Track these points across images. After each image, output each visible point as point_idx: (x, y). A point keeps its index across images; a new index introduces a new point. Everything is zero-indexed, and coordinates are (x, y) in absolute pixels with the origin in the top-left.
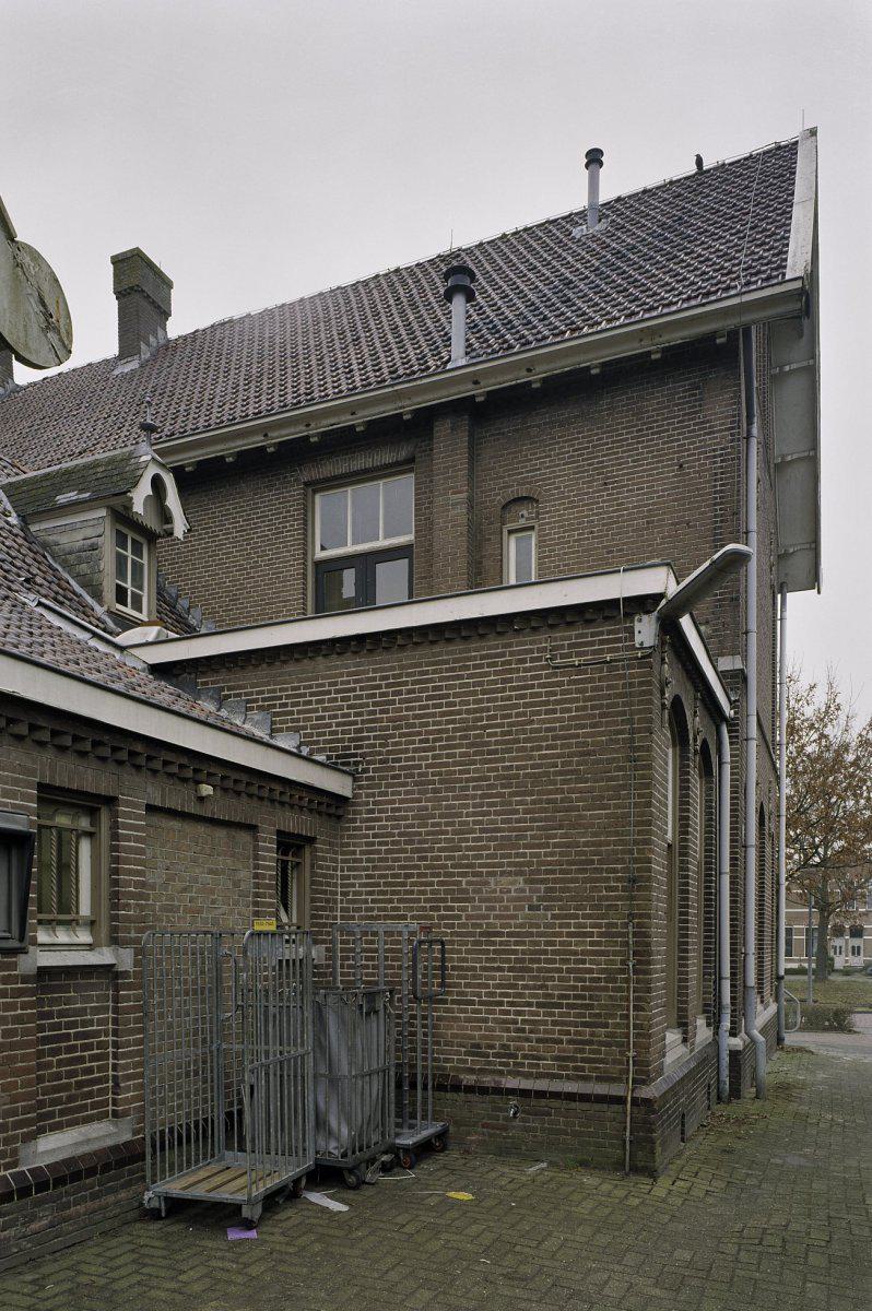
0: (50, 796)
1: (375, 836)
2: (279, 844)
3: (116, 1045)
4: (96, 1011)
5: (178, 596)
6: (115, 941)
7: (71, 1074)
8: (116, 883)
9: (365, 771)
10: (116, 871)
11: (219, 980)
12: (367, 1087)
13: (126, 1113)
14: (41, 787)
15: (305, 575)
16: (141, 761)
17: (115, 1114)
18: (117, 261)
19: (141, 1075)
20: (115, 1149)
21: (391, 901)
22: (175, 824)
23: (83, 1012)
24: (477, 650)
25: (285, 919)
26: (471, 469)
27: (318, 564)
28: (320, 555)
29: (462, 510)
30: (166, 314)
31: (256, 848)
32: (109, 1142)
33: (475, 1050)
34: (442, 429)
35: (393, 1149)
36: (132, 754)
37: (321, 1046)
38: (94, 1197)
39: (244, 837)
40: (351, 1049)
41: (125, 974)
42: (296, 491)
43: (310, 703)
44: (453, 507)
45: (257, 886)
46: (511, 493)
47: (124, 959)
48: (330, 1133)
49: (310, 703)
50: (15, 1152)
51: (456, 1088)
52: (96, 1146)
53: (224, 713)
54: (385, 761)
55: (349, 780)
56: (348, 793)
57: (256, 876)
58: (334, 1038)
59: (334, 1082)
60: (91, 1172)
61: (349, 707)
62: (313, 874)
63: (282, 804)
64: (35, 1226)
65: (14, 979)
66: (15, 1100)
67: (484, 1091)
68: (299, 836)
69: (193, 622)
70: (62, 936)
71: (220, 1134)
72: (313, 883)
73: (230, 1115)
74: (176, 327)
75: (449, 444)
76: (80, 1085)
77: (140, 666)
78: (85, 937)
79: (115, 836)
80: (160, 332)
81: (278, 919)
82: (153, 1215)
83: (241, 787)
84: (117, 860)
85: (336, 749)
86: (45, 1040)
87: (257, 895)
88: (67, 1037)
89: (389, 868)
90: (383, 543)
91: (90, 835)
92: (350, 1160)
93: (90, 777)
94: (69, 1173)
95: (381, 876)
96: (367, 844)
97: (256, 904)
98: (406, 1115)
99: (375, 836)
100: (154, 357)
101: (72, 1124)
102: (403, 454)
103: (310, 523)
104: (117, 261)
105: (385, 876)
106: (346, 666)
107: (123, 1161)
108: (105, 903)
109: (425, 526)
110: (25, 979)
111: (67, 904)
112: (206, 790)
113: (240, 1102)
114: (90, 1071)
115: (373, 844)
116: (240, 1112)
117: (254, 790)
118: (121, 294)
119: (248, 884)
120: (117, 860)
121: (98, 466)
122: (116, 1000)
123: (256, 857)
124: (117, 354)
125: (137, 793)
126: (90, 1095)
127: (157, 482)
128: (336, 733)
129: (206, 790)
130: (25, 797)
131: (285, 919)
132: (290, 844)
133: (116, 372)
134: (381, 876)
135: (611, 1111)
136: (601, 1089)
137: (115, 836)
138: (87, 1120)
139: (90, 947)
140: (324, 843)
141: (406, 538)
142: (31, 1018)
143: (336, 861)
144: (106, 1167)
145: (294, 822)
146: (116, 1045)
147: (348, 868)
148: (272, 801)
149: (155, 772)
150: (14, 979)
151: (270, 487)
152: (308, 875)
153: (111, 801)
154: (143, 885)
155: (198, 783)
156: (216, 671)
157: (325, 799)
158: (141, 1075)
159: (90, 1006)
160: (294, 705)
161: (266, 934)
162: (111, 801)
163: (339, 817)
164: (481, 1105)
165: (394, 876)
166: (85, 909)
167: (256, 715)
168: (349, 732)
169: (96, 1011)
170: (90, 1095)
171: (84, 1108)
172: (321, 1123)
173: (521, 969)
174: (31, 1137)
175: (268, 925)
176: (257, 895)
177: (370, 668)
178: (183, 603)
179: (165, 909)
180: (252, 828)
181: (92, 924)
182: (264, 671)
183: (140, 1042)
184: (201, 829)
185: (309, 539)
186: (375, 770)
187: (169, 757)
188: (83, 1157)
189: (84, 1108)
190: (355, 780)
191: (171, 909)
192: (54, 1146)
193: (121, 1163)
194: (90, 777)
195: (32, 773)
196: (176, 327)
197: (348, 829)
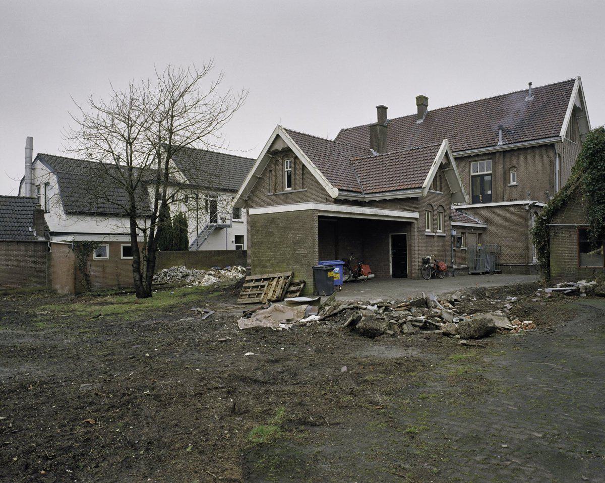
18: (417, 98)
24: (504, 209)
26: (503, 162)
27: (472, 176)
28: (473, 174)
29: (502, 169)
33: (505, 260)
34: (497, 155)
44: (500, 169)
46: (511, 166)
51: (503, 265)
67: (507, 266)
74: (429, 109)
75: (499, 158)
82: (470, 275)
90: (485, 173)
94: (464, 269)
98: (496, 269)
102: (489, 157)
104: (417, 98)
106: (486, 210)
107: (466, 269)
109: (494, 171)
132: (480, 234)
135: (524, 267)
136: (523, 264)
141: (491, 172)
145: (480, 232)
147: (487, 237)
159: (464, 252)
164: (506, 268)
173: (511, 250)
177: (489, 210)
192: (463, 266)
194: (464, 231)
196: (429, 109)
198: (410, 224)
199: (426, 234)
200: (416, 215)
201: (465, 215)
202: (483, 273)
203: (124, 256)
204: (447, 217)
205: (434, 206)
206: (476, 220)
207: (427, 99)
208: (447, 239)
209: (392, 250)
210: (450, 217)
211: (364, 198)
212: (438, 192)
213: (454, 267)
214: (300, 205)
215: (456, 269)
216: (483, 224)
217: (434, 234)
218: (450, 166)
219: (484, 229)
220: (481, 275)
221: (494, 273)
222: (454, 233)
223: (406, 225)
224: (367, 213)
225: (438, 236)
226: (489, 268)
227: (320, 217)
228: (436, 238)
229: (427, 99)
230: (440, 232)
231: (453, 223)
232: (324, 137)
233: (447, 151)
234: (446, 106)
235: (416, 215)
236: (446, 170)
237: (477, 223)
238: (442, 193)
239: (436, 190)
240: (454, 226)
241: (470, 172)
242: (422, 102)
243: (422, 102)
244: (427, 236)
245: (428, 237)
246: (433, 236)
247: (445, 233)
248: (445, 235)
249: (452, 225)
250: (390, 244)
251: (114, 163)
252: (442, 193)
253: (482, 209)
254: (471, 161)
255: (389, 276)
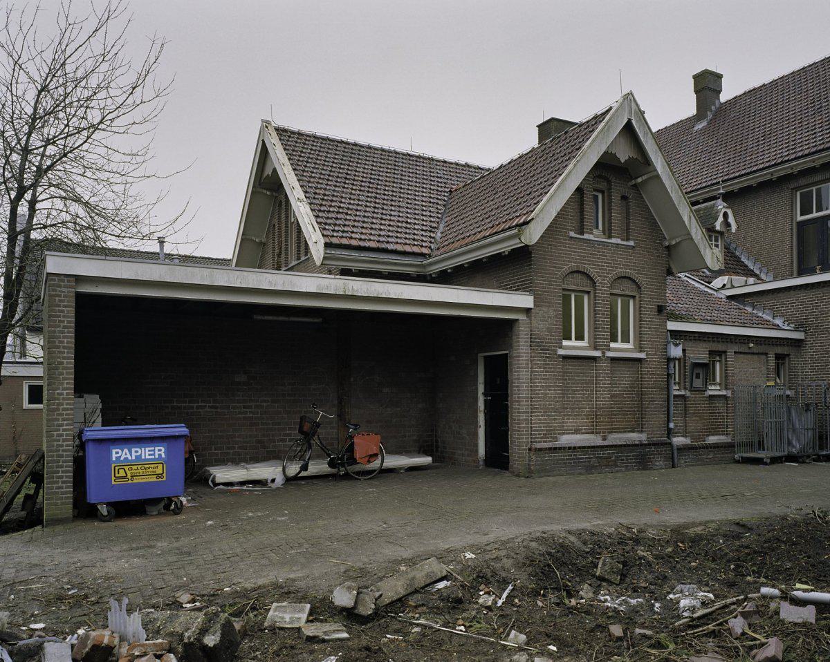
0: (712, 353)
1: (814, 352)
2: (775, 357)
3: (727, 416)
4: (722, 407)
5: (731, 243)
6: (726, 389)
7: (716, 422)
8: (726, 373)
9: (809, 330)
10: (727, 370)
11: (756, 400)
12: (806, 433)
13: (729, 434)
14: (709, 351)
15: (792, 229)
16: (733, 340)
17: (727, 434)
18: (695, 77)
19: (734, 425)
20: (727, 443)
21: (820, 374)
22: (742, 356)
23: (718, 407)
25: (778, 381)
27: (800, 224)
28: (800, 218)
30: (720, 92)
31: (727, 404)
32: (725, 441)
35: (819, 456)
36: (731, 339)
37: (790, 419)
38: (722, 454)
39: (763, 357)
40: (800, 420)
41: (729, 397)
42: (788, 193)
43: (788, 306)
45: (768, 371)
47: (729, 393)
48: (793, 446)
49: (788, 306)
50: (704, 438)
52: (722, 441)
53: (755, 312)
54: (817, 326)
55: (803, 334)
56: (803, 338)
57: (767, 369)
58: (794, 418)
59: (794, 430)
60: (722, 447)
61: (804, 308)
62: (789, 366)
63: (777, 345)
64: (709, 457)
65: (704, 397)
66: (705, 426)
68: (784, 354)
69: (738, 254)
70: (713, 388)
71: (757, 446)
72: (789, 369)
73: (759, 441)
74: (724, 97)
76: (718, 425)
77: (723, 297)
78: (718, 388)
79: (726, 361)
80: (717, 102)
81: (776, 381)
82: (738, 462)
83: (762, 342)
84: (727, 367)
85: (798, 322)
86: (710, 413)
87: (768, 374)
88: (715, 413)
89: (819, 363)
91: (719, 361)
92: (800, 454)
93: (719, 347)
95: (816, 366)
96: (811, 355)
97: (767, 377)
99: (814, 352)
100: (715, 116)
101: (716, 435)
103: (794, 209)
104: (695, 77)
105: (817, 366)
107: (729, 447)
108: (724, 379)
110: (706, 397)
111: (714, 379)
112: (751, 345)
113: (763, 438)
114: (720, 422)
115: (813, 355)
116: (763, 441)
117: (766, 342)
118: (697, 91)
119: (765, 371)
120: (727, 367)
121: (700, 210)
122: (727, 404)
123: (768, 363)
124: (695, 112)
125: (731, 350)
126: (720, 428)
127: (725, 215)
128: (798, 317)
129: (751, 345)
130: (706, 354)
131: (778, 381)
132: (779, 357)
133: (696, 128)
134: (816, 366)
137: (726, 361)
138: (720, 435)
139: (720, 390)
140: (794, 355)
142: (708, 407)
143: (799, 361)
144: (725, 447)
145: (780, 350)
146: (727, 416)
147: (803, 365)
148: (773, 345)
149: (736, 343)
150: (704, 397)
151: (774, 192)
152: (787, 365)
153: (725, 352)
154: (733, 373)
155: (748, 343)
156: (753, 297)
157: (793, 341)
158: (734, 425)
160: (782, 307)
161: (770, 386)
162: (725, 352)
163: (799, 346)
165: (821, 366)
166: (718, 380)
167: (767, 311)
168: (803, 316)
169: (722, 407)
170: (720, 428)
171: (719, 431)
172: (790, 443)
174: (708, 436)
175: (772, 383)
176: (768, 374)
177: (811, 294)
178: (733, 246)
179: (739, 380)
180: (766, 354)
181: (720, 384)
182: (770, 296)
183: (733, 416)
184: (749, 356)
185: (794, 213)
186: (813, 329)
187: (696, 335)
188: (720, 443)
189: (719, 431)
190: (806, 333)
191: (741, 380)
192: (712, 439)
193: (729, 447)
194: (719, 347)
195: (707, 348)
196: (724, 97)
197: (803, 350)
198: (511, 323)
199: (561, 352)
200: (526, 301)
201: (749, 309)
202: (774, 460)
203: (30, 402)
204: (650, 308)
205: (598, 279)
206: (779, 321)
207: (719, 77)
208: (645, 368)
209: (485, 395)
210: (660, 309)
211: (424, 266)
212: (614, 240)
213: (678, 441)
214: (86, 262)
215: (683, 449)
216: (796, 330)
217: (597, 354)
218: (651, 168)
219: (797, 343)
220: (766, 464)
221: (814, 460)
222: (676, 352)
223: (494, 332)
224: (304, 290)
225: (613, 359)
226: (796, 448)
227: (80, 297)
228: (605, 365)
229: (719, 77)
230: (621, 348)
231: (672, 326)
232: (403, 148)
233: (629, 122)
234: (758, 84)
235: (526, 301)
236: (640, 180)
237: (777, 328)
238: (631, 243)
239: (610, 237)
240: (675, 334)
241: (792, 217)
242: (707, 84)
243: (707, 84)
244: (565, 357)
245: (571, 366)
246: (594, 359)
247: (596, 349)
248: (642, 355)
249: (671, 331)
250: (481, 379)
251: (18, 230)
252: (631, 243)
253: (792, 292)
254: (796, 189)
255: (476, 461)
